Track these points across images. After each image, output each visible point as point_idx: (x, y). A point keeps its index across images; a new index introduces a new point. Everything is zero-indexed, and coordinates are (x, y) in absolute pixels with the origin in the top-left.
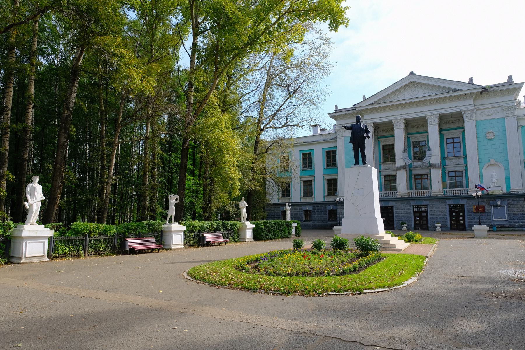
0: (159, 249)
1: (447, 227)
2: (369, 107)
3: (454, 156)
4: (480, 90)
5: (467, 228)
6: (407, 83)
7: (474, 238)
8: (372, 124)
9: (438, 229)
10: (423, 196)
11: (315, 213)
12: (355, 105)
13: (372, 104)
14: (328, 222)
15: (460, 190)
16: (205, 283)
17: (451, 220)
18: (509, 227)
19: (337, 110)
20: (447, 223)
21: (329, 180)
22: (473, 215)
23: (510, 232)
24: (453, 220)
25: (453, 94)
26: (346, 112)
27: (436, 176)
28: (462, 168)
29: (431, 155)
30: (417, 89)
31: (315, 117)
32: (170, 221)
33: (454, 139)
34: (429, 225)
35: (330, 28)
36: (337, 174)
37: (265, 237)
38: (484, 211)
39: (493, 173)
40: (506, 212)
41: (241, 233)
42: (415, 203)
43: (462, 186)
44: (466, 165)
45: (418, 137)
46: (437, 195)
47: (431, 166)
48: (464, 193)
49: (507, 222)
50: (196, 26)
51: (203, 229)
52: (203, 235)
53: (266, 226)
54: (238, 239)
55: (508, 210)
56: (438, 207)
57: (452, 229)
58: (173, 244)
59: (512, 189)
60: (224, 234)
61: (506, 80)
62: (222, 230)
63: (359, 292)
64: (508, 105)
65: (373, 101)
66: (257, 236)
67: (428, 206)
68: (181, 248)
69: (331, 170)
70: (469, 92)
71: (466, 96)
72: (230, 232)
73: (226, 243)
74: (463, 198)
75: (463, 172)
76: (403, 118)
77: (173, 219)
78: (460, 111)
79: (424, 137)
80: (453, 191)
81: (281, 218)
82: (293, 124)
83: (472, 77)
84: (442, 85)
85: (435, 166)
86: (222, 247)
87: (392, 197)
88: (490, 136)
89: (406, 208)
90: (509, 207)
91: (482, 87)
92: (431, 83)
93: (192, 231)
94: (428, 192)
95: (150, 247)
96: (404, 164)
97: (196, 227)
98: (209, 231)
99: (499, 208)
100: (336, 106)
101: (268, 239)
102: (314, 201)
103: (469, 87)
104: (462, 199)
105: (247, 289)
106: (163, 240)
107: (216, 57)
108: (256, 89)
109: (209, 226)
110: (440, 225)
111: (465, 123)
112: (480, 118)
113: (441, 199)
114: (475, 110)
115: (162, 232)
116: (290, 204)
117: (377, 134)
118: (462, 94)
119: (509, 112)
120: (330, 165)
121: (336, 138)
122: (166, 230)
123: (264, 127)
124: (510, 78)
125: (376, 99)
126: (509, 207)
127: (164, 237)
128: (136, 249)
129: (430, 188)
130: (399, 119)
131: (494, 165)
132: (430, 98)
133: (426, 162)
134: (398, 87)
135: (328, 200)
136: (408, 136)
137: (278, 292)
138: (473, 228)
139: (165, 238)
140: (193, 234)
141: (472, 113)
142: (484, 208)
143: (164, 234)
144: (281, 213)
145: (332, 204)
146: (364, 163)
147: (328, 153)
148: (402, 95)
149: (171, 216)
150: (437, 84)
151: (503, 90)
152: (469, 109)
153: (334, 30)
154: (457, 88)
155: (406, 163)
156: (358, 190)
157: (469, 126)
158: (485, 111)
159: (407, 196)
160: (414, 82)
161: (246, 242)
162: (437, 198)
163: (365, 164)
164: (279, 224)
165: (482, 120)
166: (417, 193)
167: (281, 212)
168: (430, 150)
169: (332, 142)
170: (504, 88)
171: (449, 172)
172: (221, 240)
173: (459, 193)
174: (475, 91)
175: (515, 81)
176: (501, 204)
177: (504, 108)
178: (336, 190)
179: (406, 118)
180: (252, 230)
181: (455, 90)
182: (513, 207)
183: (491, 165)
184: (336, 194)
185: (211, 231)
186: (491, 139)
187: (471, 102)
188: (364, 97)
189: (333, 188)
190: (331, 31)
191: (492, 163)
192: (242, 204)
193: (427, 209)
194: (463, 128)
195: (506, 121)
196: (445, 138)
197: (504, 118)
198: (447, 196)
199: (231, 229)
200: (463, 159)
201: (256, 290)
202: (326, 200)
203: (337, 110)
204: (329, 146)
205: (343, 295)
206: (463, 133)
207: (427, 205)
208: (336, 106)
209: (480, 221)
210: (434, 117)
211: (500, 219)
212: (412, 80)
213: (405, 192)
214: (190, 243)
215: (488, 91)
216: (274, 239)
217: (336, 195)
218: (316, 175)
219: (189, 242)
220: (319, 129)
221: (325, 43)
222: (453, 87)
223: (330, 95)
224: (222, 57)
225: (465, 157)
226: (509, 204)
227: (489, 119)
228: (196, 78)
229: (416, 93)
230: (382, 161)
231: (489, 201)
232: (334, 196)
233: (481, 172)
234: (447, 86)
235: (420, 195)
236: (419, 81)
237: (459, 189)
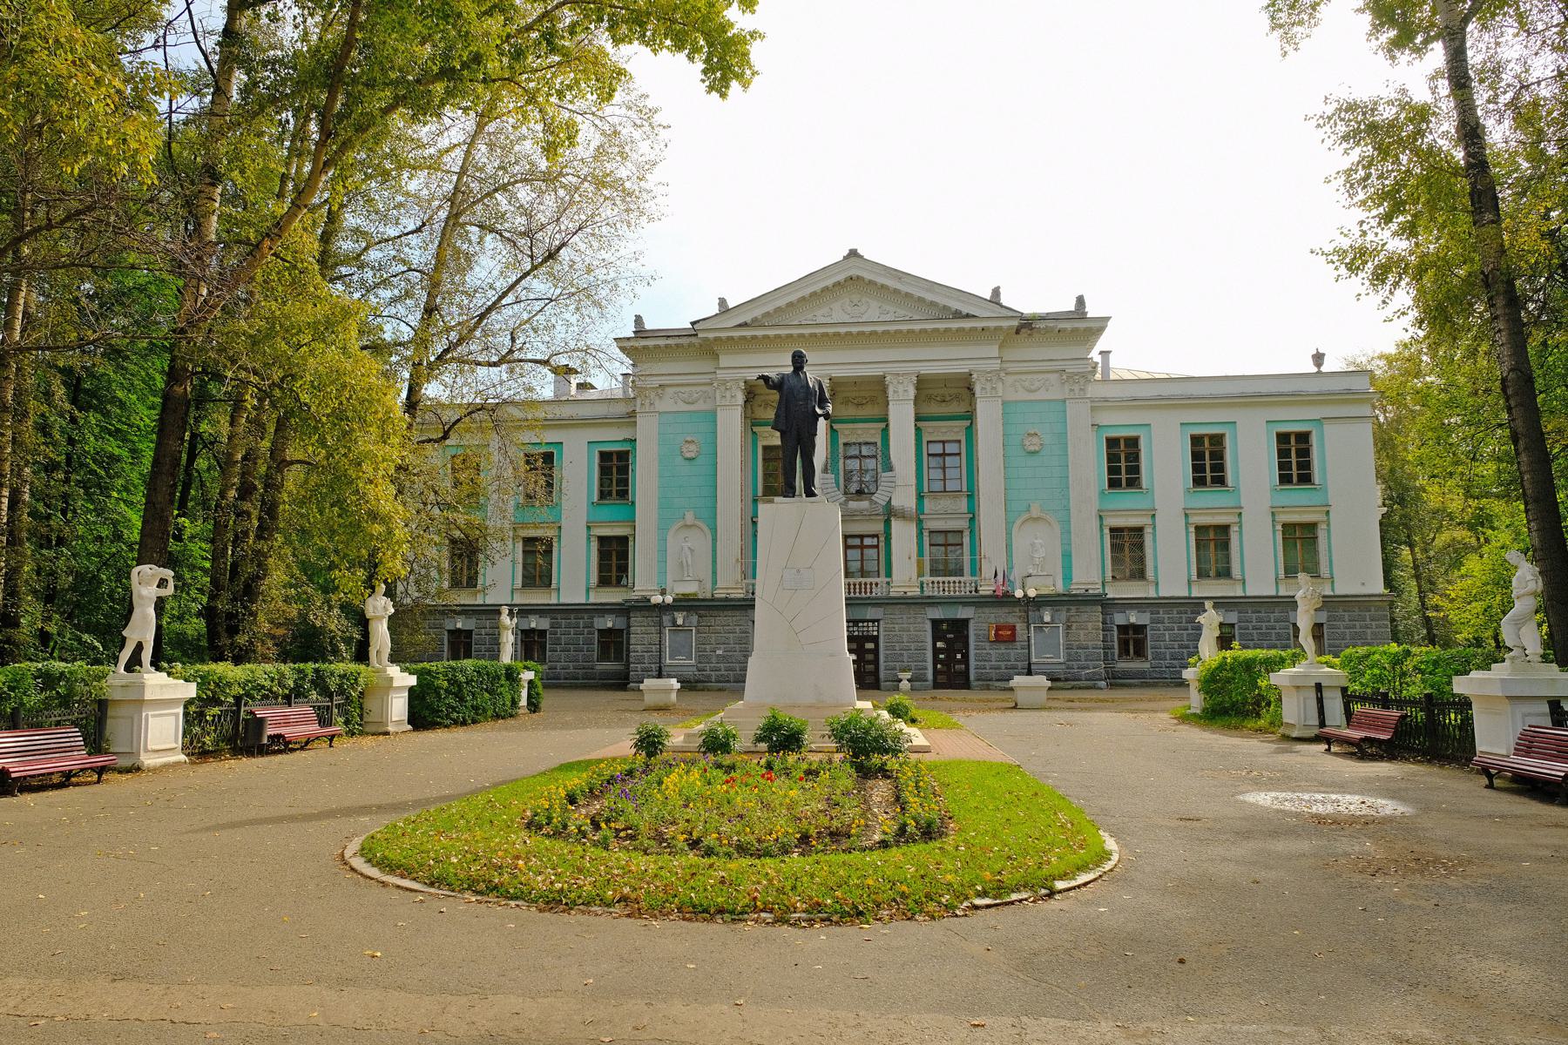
0: (101, 771)
1: (926, 681)
2: (737, 334)
3: (945, 491)
4: (1015, 323)
5: (974, 683)
6: (841, 277)
7: (1015, 707)
8: (742, 385)
9: (905, 685)
10: (858, 594)
11: (559, 639)
12: (698, 321)
13: (744, 325)
14: (597, 667)
16: (513, 903)
17: (936, 661)
18: (1067, 680)
19: (640, 332)
20: (926, 669)
22: (988, 648)
23: (1069, 692)
24: (941, 662)
26: (670, 341)
27: (904, 537)
28: (961, 524)
31: (598, 342)
32: (134, 663)
34: (882, 675)
35: (703, 81)
36: (848, 517)
37: (448, 716)
38: (1012, 638)
41: (369, 704)
42: (937, 613)
43: (960, 572)
45: (860, 432)
47: (889, 513)
48: (965, 591)
51: (252, 691)
52: (252, 713)
53: (453, 681)
54: (360, 725)
56: (905, 626)
57: (937, 685)
58: (146, 751)
60: (319, 707)
62: (314, 695)
63: (1046, 891)
64: (1076, 371)
65: (747, 318)
66: (423, 714)
67: (881, 622)
68: (178, 763)
69: (611, 511)
70: (992, 324)
71: (984, 334)
72: (338, 700)
73: (331, 740)
74: (965, 602)
75: (964, 534)
76: (827, 375)
77: (147, 655)
78: (967, 371)
79: (873, 432)
80: (944, 582)
81: (445, 654)
82: (529, 356)
83: (999, 287)
84: (929, 297)
85: (903, 515)
86: (319, 753)
87: (858, 594)
88: (1032, 444)
90: (1069, 627)
91: (1021, 316)
92: (904, 288)
93: (214, 701)
94: (877, 584)
95: (66, 764)
97: (229, 685)
98: (269, 697)
99: (1046, 630)
100: (638, 320)
101: (455, 722)
102: (555, 602)
103: (994, 312)
105: (705, 911)
106: (107, 733)
107: (332, 99)
108: (418, 230)
109: (272, 680)
110: (908, 675)
111: (890, 406)
112: (1011, 396)
114: (1002, 374)
115: (103, 705)
116: (516, 610)
117: (749, 412)
118: (976, 329)
119: (1076, 387)
120: (610, 493)
121: (632, 415)
122: (117, 695)
123: (439, 358)
124: (1080, 301)
125: (758, 313)
126: (1069, 627)
127: (110, 724)
128: (13, 775)
129: (882, 572)
131: (1038, 519)
132: (910, 327)
133: (878, 501)
134: (817, 287)
135: (599, 601)
136: (831, 427)
137: (818, 914)
138: (1012, 683)
139: (115, 727)
140: (216, 710)
142: (1013, 629)
143: (110, 712)
144: (446, 638)
145: (535, 614)
146: (810, 493)
147: (605, 456)
148: (825, 310)
149: (140, 647)
150: (917, 293)
151: (1065, 330)
153: (717, 91)
154: (965, 311)
156: (798, 571)
157: (987, 413)
158: (683, 389)
159: (742, 596)
160: (858, 277)
161: (387, 733)
162: (905, 602)
163: (813, 495)
164: (488, 674)
165: (1016, 402)
166: (852, 587)
167: (446, 633)
169: (619, 425)
170: (1068, 325)
171: (931, 532)
172: (314, 728)
175: (1092, 311)
176: (1053, 621)
177: (1064, 377)
178: (623, 569)
179: (922, 372)
180: (407, 694)
181: (958, 315)
184: (624, 582)
185: (276, 698)
187: (993, 351)
188: (722, 302)
189: (614, 565)
190: (709, 92)
191: (1035, 513)
192: (375, 607)
193: (878, 631)
194: (970, 416)
195: (1068, 409)
196: (842, 440)
197: (1064, 401)
198: (929, 597)
199: (341, 691)
200: (965, 500)
201: (741, 913)
202: (592, 600)
203: (640, 332)
204: (612, 437)
205: (1012, 903)
206: (886, 430)
207: (878, 621)
208: (638, 320)
210: (906, 382)
212: (854, 272)
214: (204, 743)
215: (1032, 329)
216: (474, 722)
217: (624, 586)
218: (564, 523)
219: (198, 742)
220: (575, 380)
221: (639, 122)
222: (955, 305)
223: (651, 282)
224: (353, 100)
225: (972, 495)
227: (1031, 401)
228: (236, 157)
230: (760, 493)
232: (618, 589)
233: (1009, 534)
234: (941, 300)
235: (860, 593)
237: (952, 579)
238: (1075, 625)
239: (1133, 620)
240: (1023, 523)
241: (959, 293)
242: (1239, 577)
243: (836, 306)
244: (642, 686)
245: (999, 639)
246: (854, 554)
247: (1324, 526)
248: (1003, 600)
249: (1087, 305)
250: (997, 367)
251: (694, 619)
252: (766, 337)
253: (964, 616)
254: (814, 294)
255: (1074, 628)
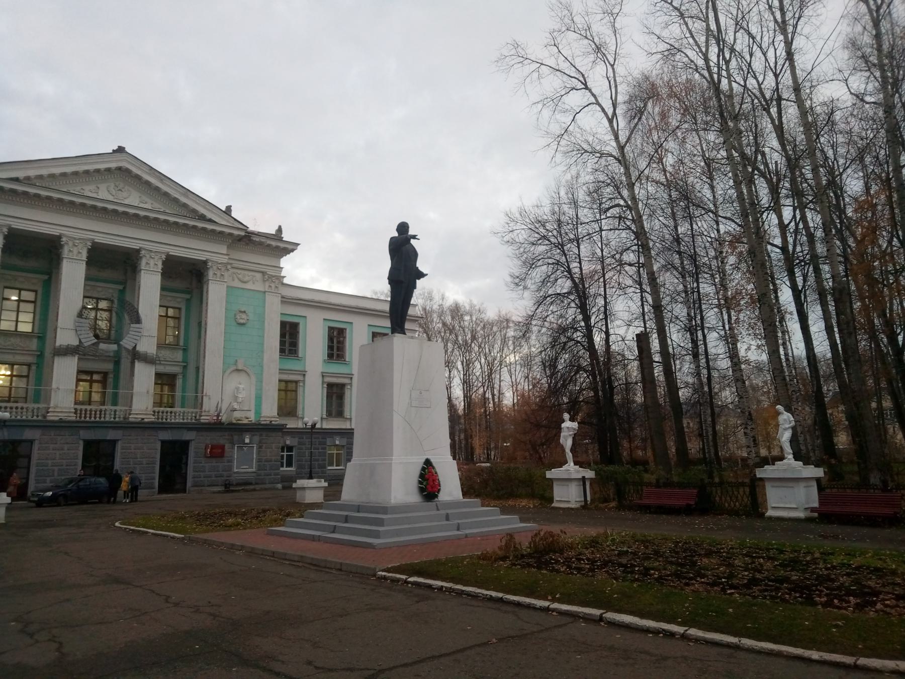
10: (98, 419)
13: (16, 180)
15: (158, 412)
21: (330, 386)
25: (200, 225)
29: (140, 334)
30: (126, 187)
33: (22, 292)
38: (221, 455)
39: (240, 386)
40: (255, 456)
44: (185, 364)
46: (143, 419)
49: (253, 475)
50: (807, 195)
55: (259, 453)
59: (264, 417)
61: (272, 231)
70: (227, 230)
74: (115, 426)
76: (89, 240)
78: (58, 234)
83: (231, 206)
84: (183, 200)
88: (242, 318)
89: (66, 447)
91: (244, 228)
92: (164, 188)
96: (75, 342)
103: (228, 222)
104: (188, 430)
113: (65, 427)
124: (280, 230)
125: (32, 173)
130: (79, 239)
132: (137, 212)
135: (328, 427)
141: (223, 269)
152: (220, 262)
155: (80, 341)
158: (239, 271)
162: (142, 427)
168: (138, 320)
173: (160, 417)
174: (236, 232)
175: (286, 237)
179: (171, 253)
181: (203, 218)
182: (266, 448)
183: (238, 370)
186: (243, 324)
187: (223, 249)
197: (265, 292)
209: (311, 471)
211: (245, 469)
213: (70, 408)
222: (202, 210)
226: (260, 442)
227: (243, 289)
229: (125, 194)
231: (232, 436)
236: (139, 173)
238: (264, 445)
239: (288, 442)
240: (231, 373)
241: (207, 203)
242: (348, 417)
243: (103, 187)
244: (294, 485)
245: (213, 455)
246: (83, 386)
247: (301, 384)
248: (217, 426)
249: (283, 232)
250: (225, 261)
251: (256, 438)
252: (37, 196)
253: (187, 438)
254: (87, 172)
255: (263, 447)
